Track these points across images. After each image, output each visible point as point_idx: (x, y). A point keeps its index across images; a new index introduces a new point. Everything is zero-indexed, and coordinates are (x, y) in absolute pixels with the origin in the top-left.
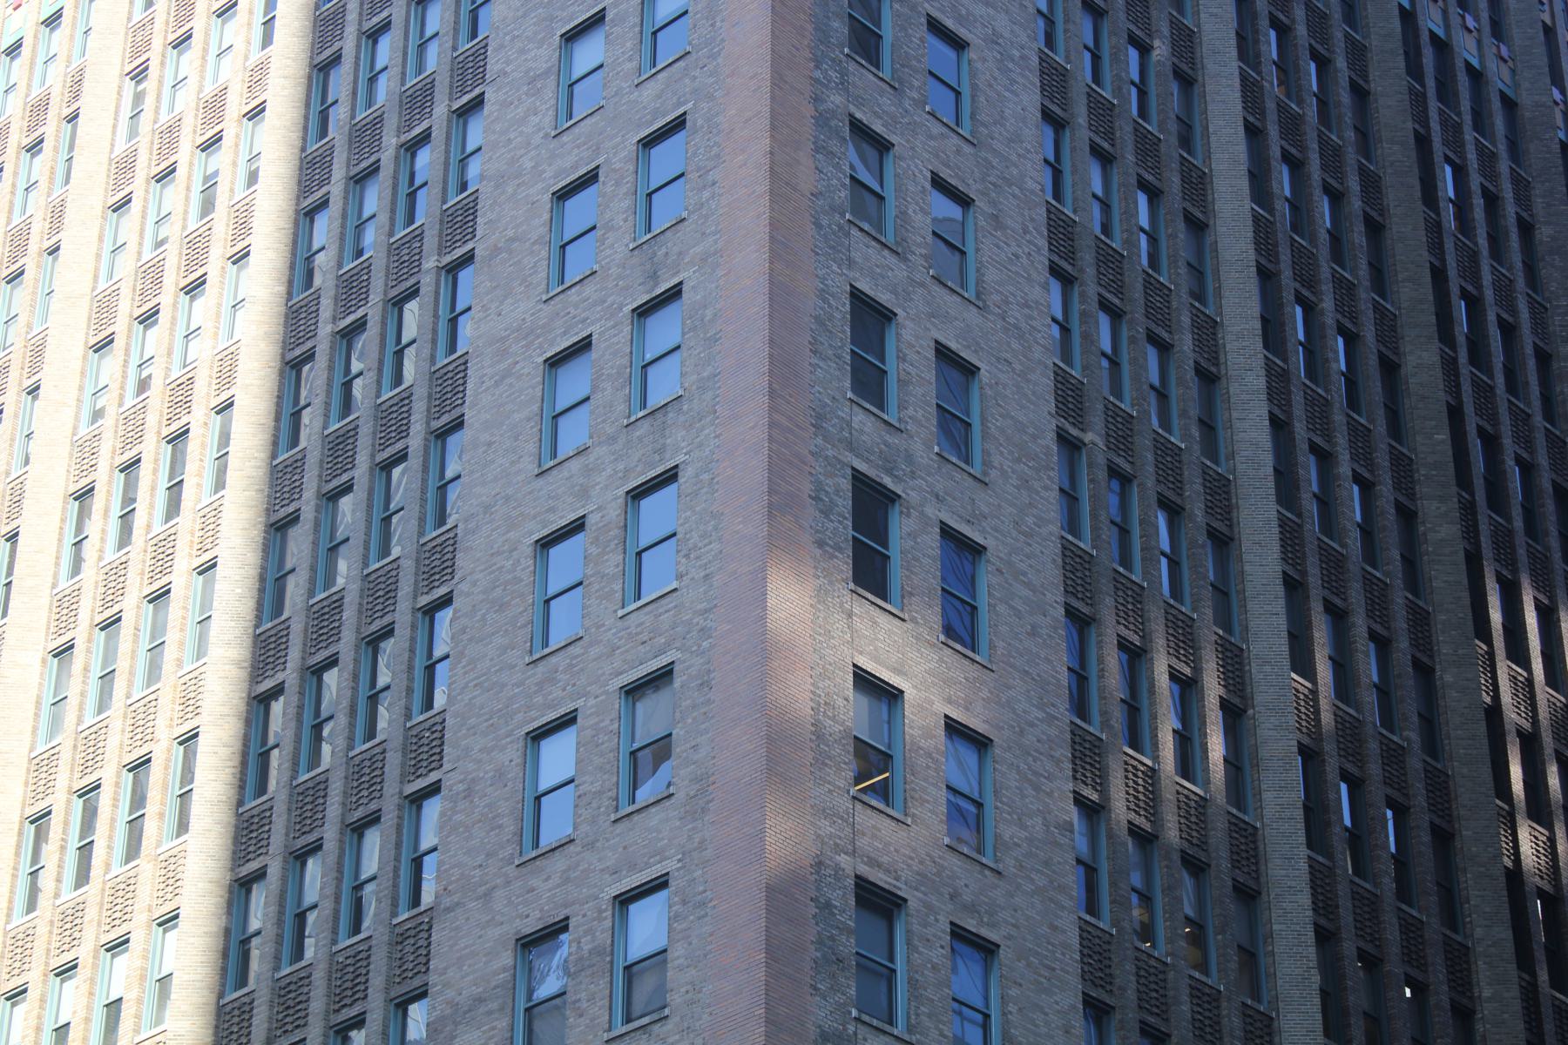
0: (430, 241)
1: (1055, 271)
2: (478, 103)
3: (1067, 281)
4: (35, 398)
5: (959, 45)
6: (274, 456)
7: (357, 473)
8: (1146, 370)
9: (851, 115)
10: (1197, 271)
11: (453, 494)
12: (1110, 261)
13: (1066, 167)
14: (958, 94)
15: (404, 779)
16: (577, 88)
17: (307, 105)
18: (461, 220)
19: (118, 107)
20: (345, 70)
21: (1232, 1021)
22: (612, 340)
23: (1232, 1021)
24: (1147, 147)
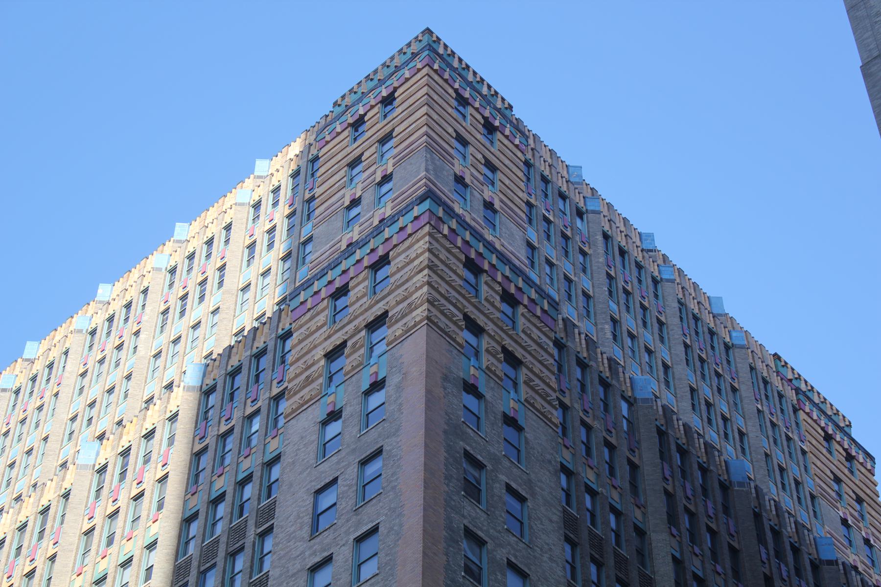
0: (251, 523)
1: (567, 539)
2: (270, 529)
3: (573, 545)
4: (53, 562)
5: (522, 499)
6: (176, 560)
7: (218, 559)
8: (609, 523)
9: (465, 450)
10: (640, 553)
11: (274, 487)
12: (597, 543)
13: (578, 565)
14: (522, 523)
15: (257, 526)
16: (327, 445)
17: (190, 469)
18: (268, 513)
19: (90, 487)
20: (210, 454)
21: (634, 576)
22: (344, 555)
23: (634, 576)
24: (621, 562)
